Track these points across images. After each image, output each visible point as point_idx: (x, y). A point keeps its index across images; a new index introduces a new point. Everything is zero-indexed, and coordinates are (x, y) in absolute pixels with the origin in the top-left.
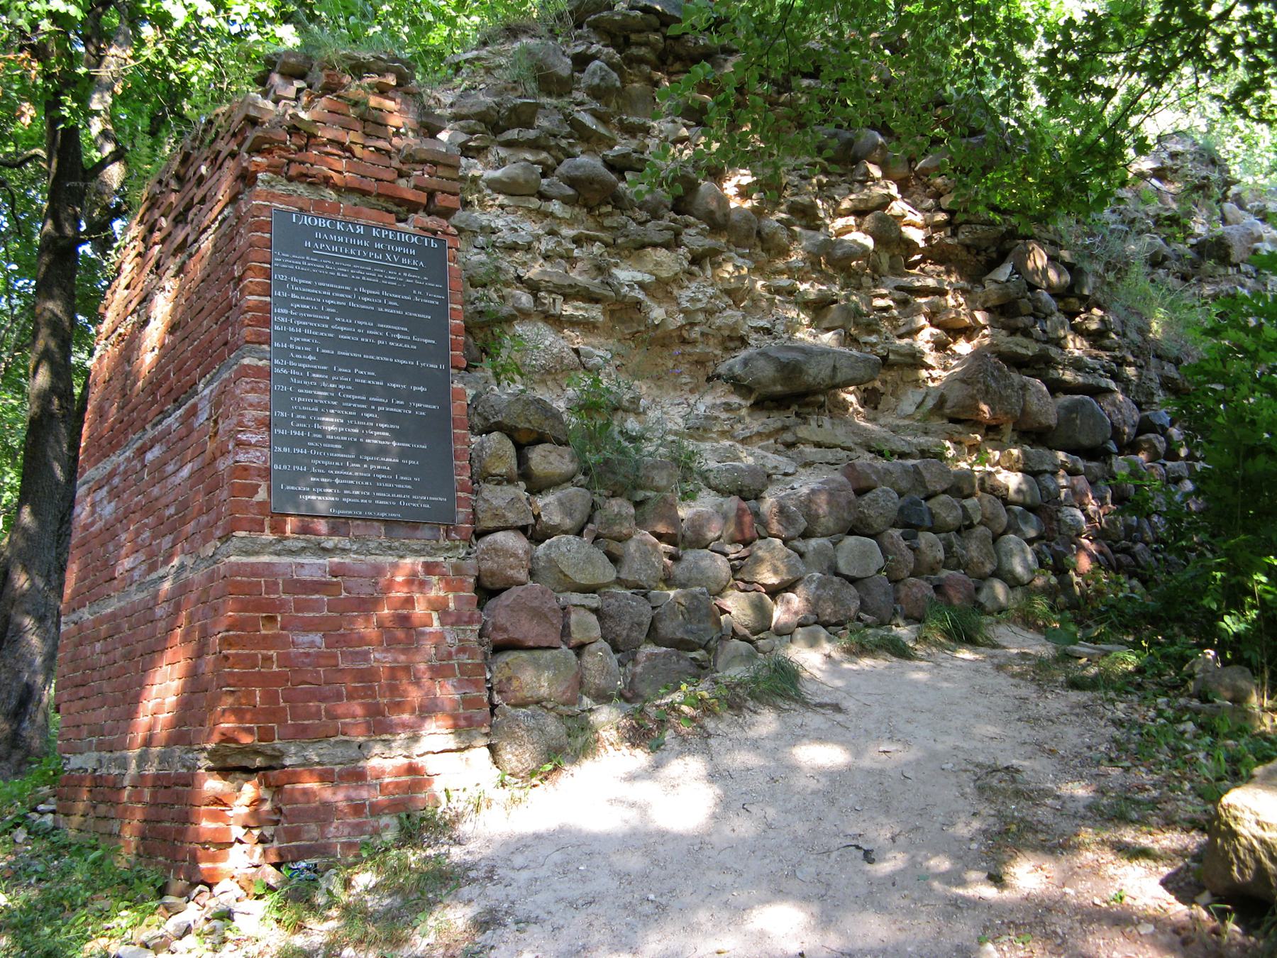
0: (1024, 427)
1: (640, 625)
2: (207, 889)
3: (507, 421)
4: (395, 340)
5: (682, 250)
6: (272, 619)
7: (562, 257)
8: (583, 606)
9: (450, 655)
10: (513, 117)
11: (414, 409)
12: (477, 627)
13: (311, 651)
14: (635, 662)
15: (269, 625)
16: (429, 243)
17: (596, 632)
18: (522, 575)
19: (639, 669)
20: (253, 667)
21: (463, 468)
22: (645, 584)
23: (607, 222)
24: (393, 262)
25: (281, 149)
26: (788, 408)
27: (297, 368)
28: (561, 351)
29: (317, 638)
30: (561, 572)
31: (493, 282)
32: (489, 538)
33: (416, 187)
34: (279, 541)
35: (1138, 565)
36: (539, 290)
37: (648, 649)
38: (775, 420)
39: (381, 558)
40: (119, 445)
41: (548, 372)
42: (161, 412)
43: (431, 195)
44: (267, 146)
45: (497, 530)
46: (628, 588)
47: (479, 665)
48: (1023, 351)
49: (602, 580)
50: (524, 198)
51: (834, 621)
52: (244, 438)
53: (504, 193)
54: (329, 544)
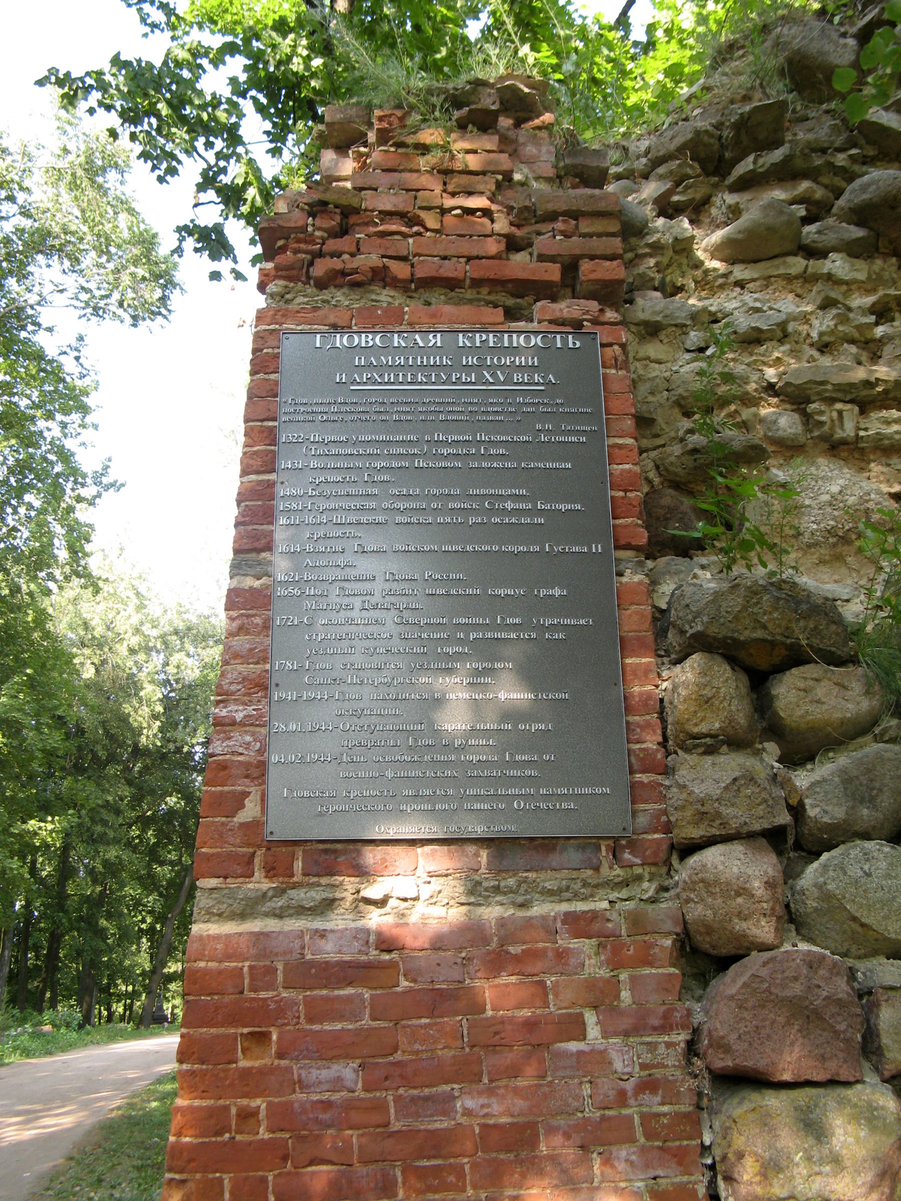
3: (713, 630)
6: (262, 1038)
7: (852, 341)
9: (622, 1098)
10: (744, 138)
11: (543, 628)
12: (681, 1037)
13: (336, 1097)
16: (565, 341)
20: (219, 1133)
21: (647, 726)
24: (497, 382)
25: (299, 241)
28: (863, 500)
29: (347, 1071)
30: (854, 919)
31: (724, 402)
32: (694, 860)
34: (280, 892)
41: (845, 540)
47: (686, 1115)
50: (776, 262)
52: (224, 713)
53: (743, 262)
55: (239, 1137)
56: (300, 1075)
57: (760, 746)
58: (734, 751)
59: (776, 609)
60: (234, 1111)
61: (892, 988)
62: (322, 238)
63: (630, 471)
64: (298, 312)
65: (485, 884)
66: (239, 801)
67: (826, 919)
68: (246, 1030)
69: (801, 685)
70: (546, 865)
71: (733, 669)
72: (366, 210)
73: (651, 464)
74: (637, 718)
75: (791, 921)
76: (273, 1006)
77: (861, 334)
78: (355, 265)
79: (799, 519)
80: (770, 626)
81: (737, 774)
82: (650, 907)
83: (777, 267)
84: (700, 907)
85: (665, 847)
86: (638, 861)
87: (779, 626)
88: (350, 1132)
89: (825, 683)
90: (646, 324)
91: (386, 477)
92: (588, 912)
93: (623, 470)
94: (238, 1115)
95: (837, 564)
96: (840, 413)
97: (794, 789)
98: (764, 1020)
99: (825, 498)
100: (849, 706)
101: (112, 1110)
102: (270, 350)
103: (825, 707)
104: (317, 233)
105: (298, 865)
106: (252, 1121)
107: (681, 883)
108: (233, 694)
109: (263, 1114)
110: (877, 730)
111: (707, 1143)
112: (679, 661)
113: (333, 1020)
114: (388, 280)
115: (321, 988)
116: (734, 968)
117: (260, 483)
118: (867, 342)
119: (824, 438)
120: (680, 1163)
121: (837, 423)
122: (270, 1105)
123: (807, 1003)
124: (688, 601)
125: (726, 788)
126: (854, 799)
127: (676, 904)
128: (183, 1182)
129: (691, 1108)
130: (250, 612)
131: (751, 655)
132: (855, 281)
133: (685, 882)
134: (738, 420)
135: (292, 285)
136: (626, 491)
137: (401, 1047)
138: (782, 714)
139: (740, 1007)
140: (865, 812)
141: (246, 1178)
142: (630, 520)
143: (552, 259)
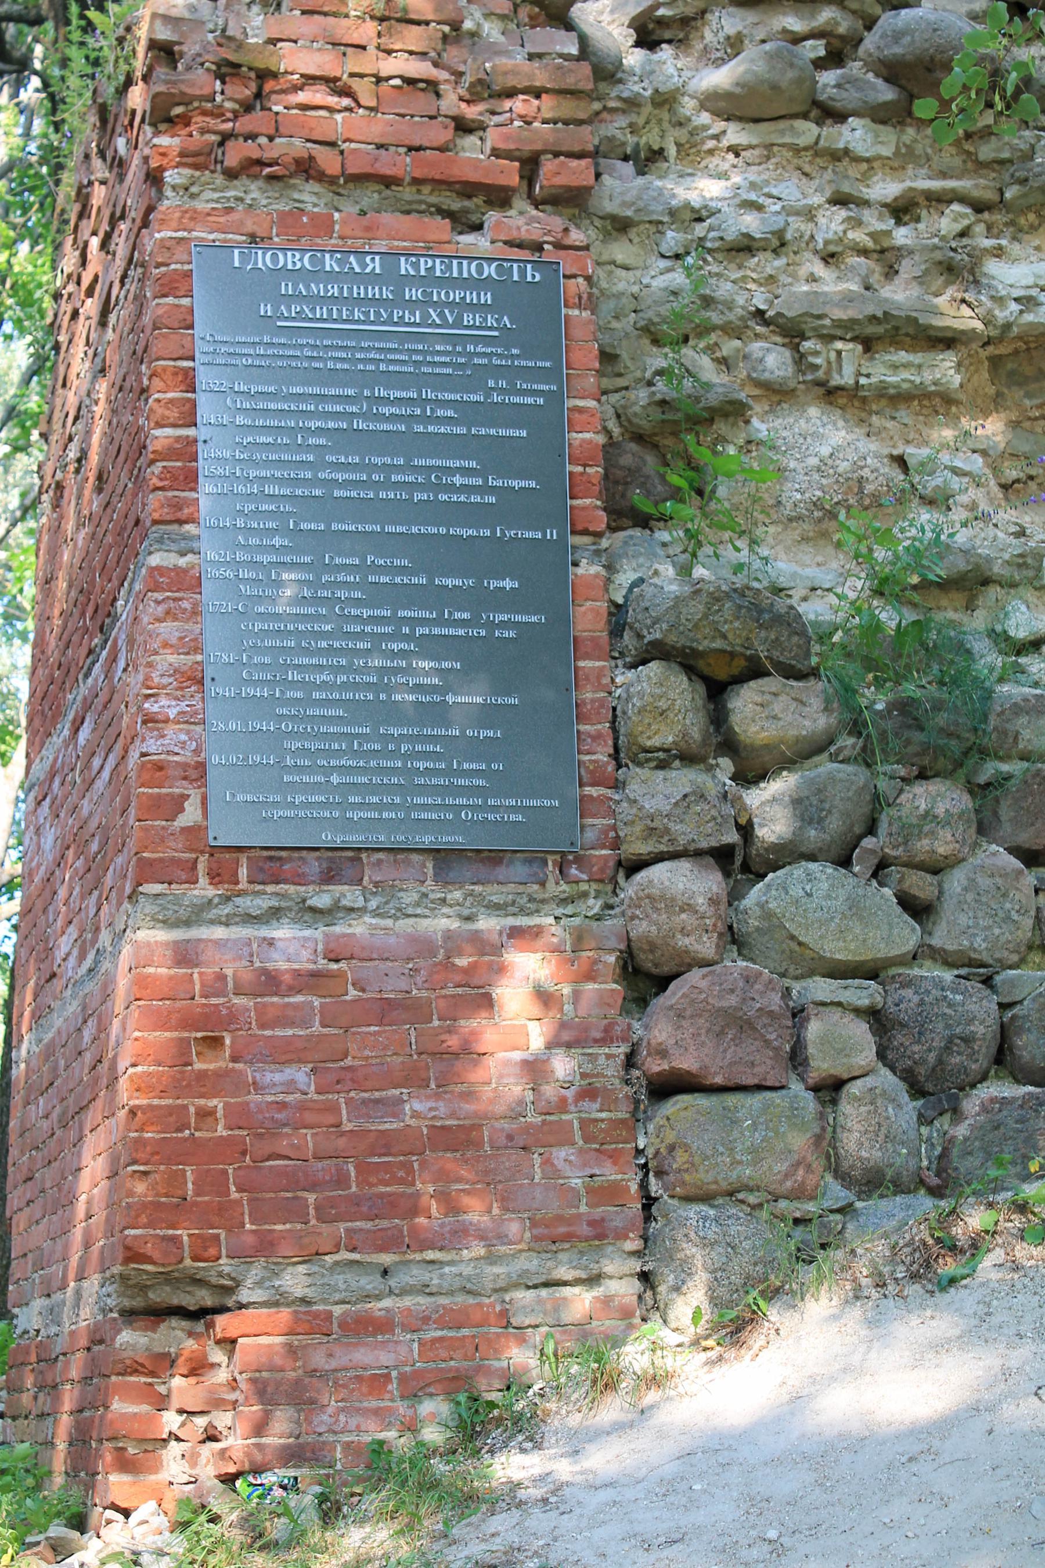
1: (967, 1040)
2: (120, 1517)
3: (672, 639)
4: (452, 488)
6: (215, 1042)
7: (864, 252)
8: (839, 1004)
11: (491, 625)
12: (621, 1050)
13: (290, 1098)
14: (956, 1113)
15: (209, 1054)
16: (523, 273)
17: (866, 1054)
18: (706, 946)
19: (961, 1131)
20: (179, 1130)
21: (597, 737)
22: (986, 957)
23: (986, 151)
24: (445, 324)
25: (205, 113)
27: (254, 564)
28: (857, 467)
29: (300, 1075)
30: (793, 937)
31: (704, 330)
33: (496, 153)
39: (425, 923)
43: (530, 164)
44: (178, 110)
45: (659, 858)
46: (949, 964)
47: (623, 1121)
49: (883, 951)
50: (782, 124)
52: (155, 708)
53: (740, 119)
54: (322, 901)
55: (197, 1134)
56: (254, 1077)
57: (714, 762)
58: (685, 766)
59: (738, 618)
60: (192, 1110)
61: (823, 1004)
62: (235, 112)
63: (590, 442)
64: (209, 214)
65: (432, 896)
66: (178, 804)
67: (766, 938)
68: (199, 1035)
69: (759, 700)
70: (492, 878)
71: (690, 679)
72: (286, 72)
73: (611, 411)
74: (588, 727)
75: (734, 941)
76: (224, 1012)
77: (875, 241)
78: (274, 154)
79: (782, 485)
80: (730, 636)
81: (688, 790)
82: (595, 924)
83: (782, 132)
84: (645, 923)
85: (611, 864)
86: (585, 877)
87: (740, 636)
88: (304, 1131)
89: (783, 698)
90: (614, 218)
91: (322, 441)
93: (583, 440)
94: (197, 1114)
95: (822, 542)
96: (839, 353)
97: (744, 808)
98: (699, 1028)
99: (813, 461)
100: (807, 723)
102: (178, 266)
103: (781, 723)
104: (228, 105)
105: (243, 873)
106: (210, 1119)
107: (627, 901)
108: (164, 687)
109: (220, 1113)
110: (833, 749)
111: (641, 1147)
112: (634, 666)
113: (284, 1026)
114: (312, 172)
115: (272, 995)
116: (672, 986)
117: (178, 439)
118: (882, 251)
119: (819, 383)
120: (615, 1163)
121: (834, 365)
122: (226, 1105)
123: (741, 1014)
124: (648, 604)
125: (676, 804)
126: (803, 820)
127: (621, 921)
128: (145, 1173)
129: (628, 1115)
130: (177, 595)
131: (709, 665)
132: (879, 157)
133: (631, 898)
134: (718, 354)
135: (197, 173)
136: (585, 466)
137: (352, 1052)
138: (737, 729)
139: (679, 1016)
140: (813, 833)
141: (208, 1171)
142: (588, 501)
143: (508, 155)
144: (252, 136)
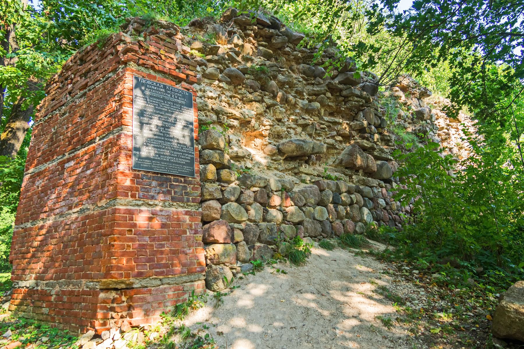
0: (366, 171)
5: (264, 104)
8: (238, 228)
15: (129, 233)
18: (218, 216)
26: (295, 160)
31: (204, 110)
32: (207, 203)
35: (401, 220)
36: (219, 114)
37: (258, 244)
38: (292, 165)
40: (48, 160)
42: (74, 149)
48: (366, 145)
51: (314, 235)
54: (151, 203)
92: (4, 272)
101: (192, 206)
144: (144, 59)
